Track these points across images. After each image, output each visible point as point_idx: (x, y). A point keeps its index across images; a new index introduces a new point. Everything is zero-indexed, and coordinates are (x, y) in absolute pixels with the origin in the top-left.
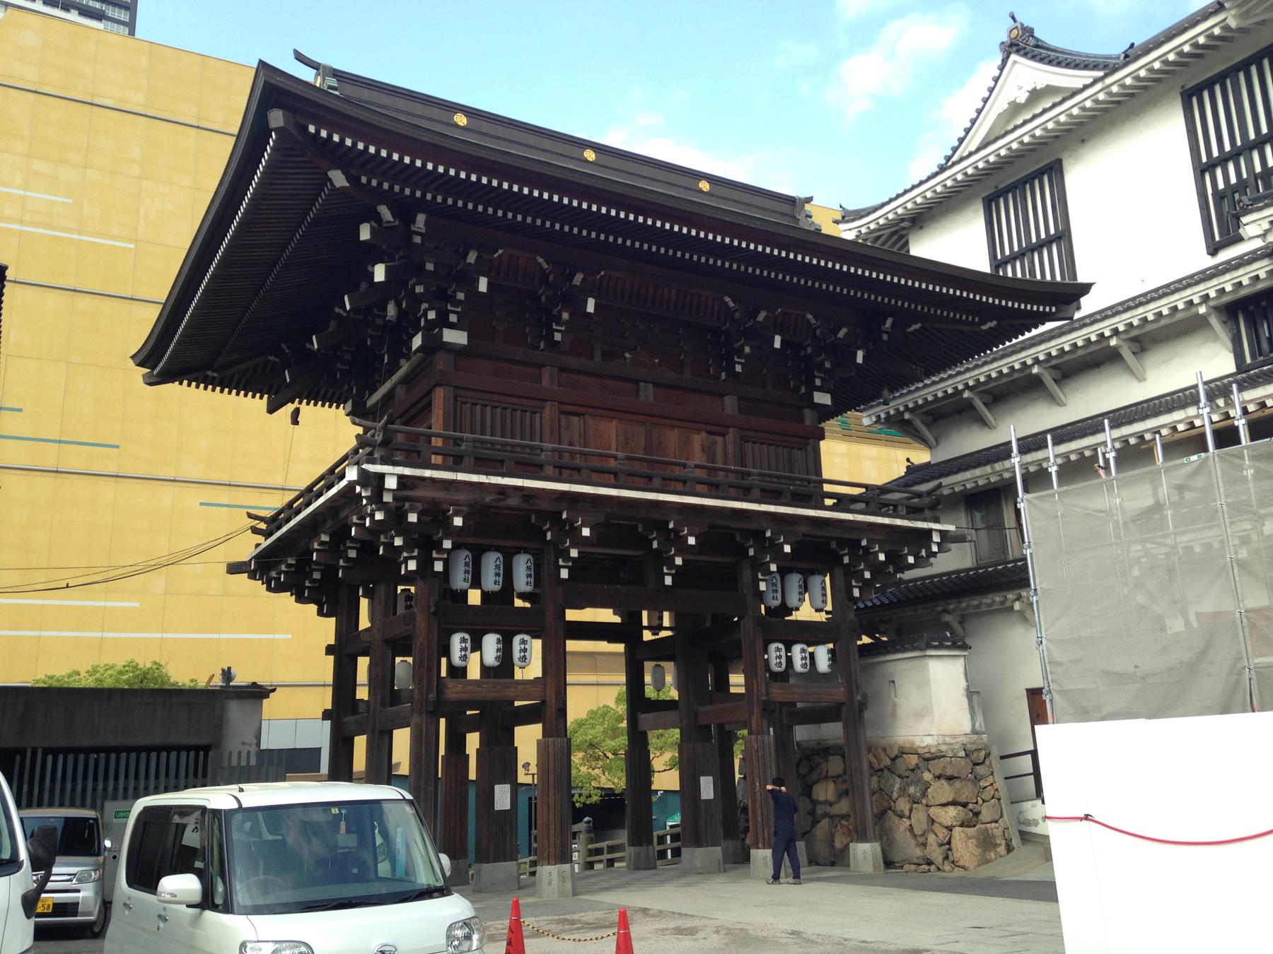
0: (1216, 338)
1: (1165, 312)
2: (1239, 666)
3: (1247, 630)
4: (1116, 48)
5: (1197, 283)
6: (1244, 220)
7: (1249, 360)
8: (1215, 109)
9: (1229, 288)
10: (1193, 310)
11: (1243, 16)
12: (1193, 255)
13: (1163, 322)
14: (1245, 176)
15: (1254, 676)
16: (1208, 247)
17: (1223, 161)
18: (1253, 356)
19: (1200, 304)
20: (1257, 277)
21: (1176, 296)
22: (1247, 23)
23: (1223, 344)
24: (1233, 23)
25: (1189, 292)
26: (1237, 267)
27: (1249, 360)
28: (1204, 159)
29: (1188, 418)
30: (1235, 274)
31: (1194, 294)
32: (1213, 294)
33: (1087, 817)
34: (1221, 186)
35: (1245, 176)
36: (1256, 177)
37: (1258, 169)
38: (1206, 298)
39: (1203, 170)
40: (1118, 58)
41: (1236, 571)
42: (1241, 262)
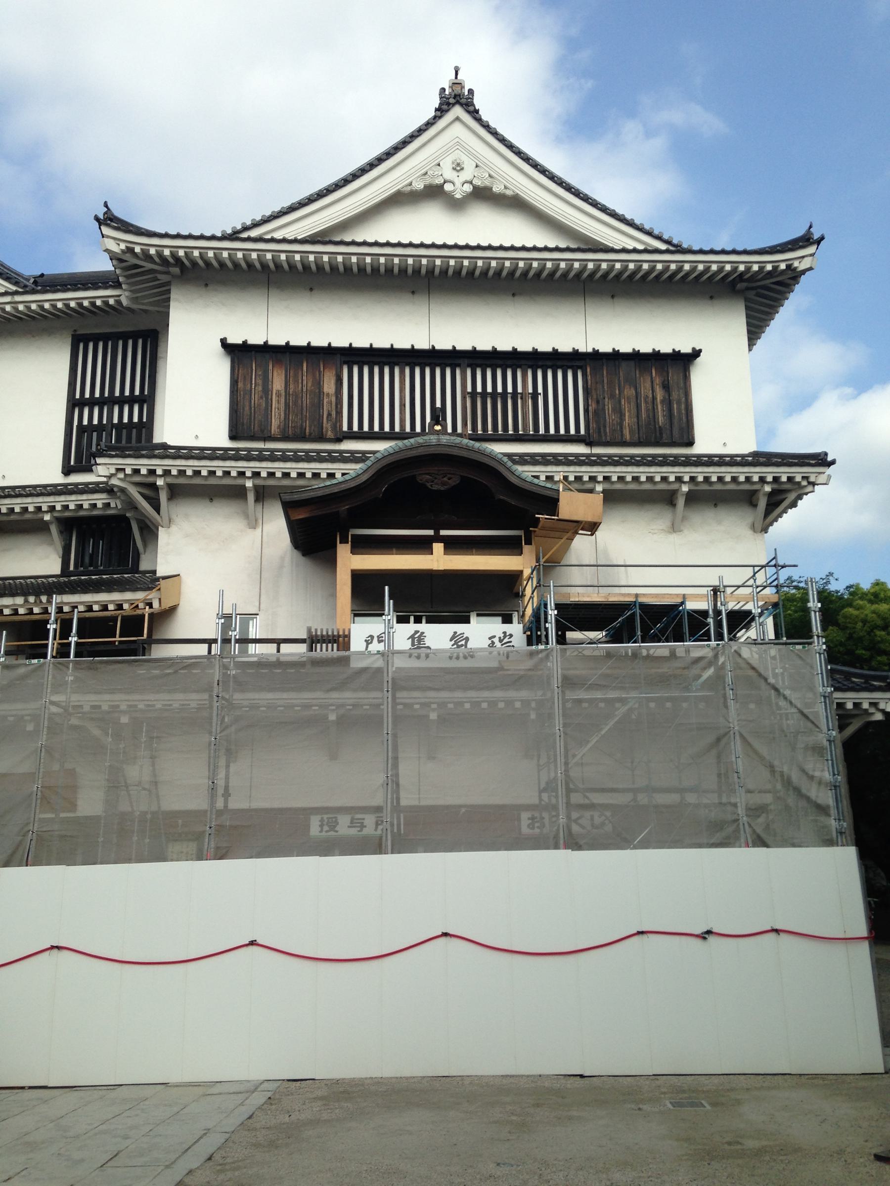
0: (51, 543)
1: (17, 509)
2: (26, 829)
3: (39, 801)
4: (29, 269)
5: (49, 494)
6: (99, 460)
7: (72, 568)
8: (95, 360)
9: (72, 507)
10: (40, 515)
11: (134, 300)
12: (51, 473)
13: (13, 517)
14: (105, 422)
15: (34, 838)
16: (63, 467)
17: (92, 403)
18: (76, 566)
19: (47, 512)
20: (95, 505)
21: (29, 500)
22: (134, 307)
23: (56, 550)
24: (125, 302)
25: (40, 499)
26: (82, 492)
27: (72, 568)
28: (78, 396)
29: (15, 605)
30: (80, 497)
31: (45, 502)
32: (58, 507)
33: (252, 943)
34: (85, 422)
35: (105, 422)
36: (113, 425)
37: (116, 421)
38: (52, 509)
39: (74, 404)
40: (28, 280)
41: (43, 754)
42: (85, 489)
